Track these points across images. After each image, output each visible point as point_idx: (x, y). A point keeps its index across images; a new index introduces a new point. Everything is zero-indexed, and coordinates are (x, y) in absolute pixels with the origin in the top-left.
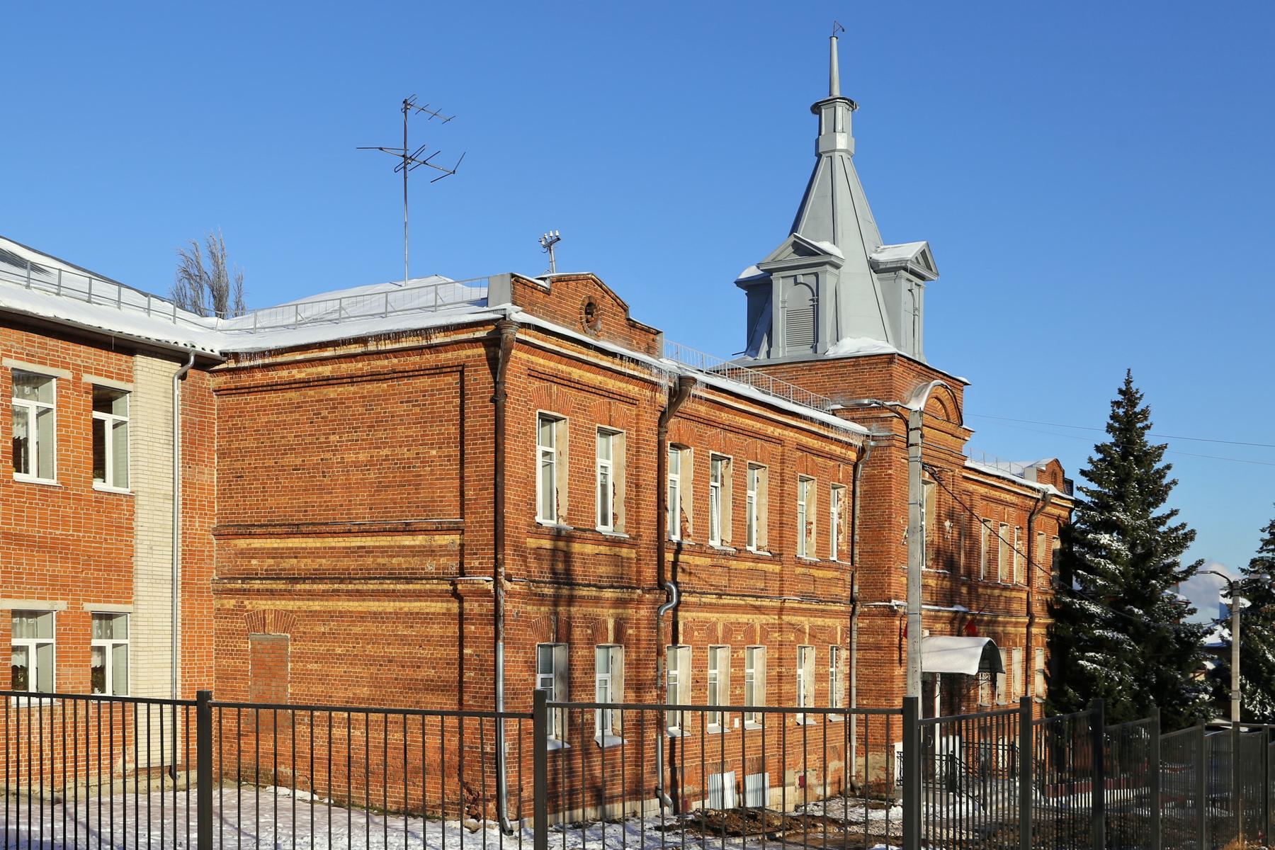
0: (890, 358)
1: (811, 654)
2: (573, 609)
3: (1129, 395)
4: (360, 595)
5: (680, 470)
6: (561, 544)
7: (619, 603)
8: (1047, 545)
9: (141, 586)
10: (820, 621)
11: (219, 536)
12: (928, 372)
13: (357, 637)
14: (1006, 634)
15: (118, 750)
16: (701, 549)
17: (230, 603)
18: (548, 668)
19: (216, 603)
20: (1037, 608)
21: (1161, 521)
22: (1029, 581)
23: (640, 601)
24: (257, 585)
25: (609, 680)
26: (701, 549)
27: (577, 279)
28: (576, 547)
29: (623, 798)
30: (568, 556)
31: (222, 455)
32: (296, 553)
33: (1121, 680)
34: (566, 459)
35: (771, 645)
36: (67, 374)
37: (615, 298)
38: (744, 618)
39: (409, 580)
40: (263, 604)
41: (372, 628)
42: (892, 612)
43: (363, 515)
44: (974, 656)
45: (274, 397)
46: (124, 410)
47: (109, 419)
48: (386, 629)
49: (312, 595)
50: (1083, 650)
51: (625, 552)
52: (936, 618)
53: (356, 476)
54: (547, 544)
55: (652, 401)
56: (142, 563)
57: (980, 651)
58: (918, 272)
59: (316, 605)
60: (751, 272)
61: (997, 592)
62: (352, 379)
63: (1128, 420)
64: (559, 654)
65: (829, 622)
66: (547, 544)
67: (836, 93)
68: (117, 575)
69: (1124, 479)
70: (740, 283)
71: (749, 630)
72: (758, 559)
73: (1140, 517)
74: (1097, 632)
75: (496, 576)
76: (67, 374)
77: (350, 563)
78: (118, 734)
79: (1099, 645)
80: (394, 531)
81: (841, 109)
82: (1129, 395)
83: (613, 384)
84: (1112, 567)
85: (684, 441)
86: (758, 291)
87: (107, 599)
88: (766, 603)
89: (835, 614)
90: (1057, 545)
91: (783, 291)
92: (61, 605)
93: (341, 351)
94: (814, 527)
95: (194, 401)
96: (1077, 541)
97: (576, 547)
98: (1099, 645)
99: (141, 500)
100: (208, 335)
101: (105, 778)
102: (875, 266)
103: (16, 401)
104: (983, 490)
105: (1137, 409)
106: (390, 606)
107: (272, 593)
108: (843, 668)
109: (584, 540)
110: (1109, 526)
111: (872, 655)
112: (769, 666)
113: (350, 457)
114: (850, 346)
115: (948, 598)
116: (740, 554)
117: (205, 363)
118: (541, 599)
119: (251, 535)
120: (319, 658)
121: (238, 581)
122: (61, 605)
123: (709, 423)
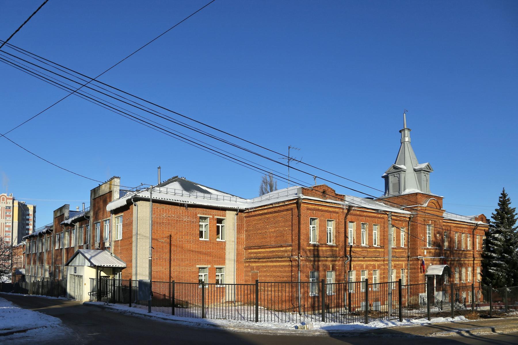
0: (417, 194)
1: (395, 271)
2: (320, 263)
3: (504, 195)
4: (272, 262)
5: (352, 228)
6: (316, 248)
7: (332, 261)
8: (479, 240)
9: (227, 261)
10: (397, 263)
11: (245, 249)
12: (429, 196)
13: (272, 271)
14: (465, 264)
15: (221, 297)
16: (358, 247)
17: (247, 264)
18: (313, 277)
19: (245, 265)
20: (477, 255)
21: (515, 229)
22: (473, 248)
23: (339, 260)
24: (252, 260)
25: (331, 278)
26: (358, 247)
27: (320, 186)
28: (320, 248)
29: (334, 308)
30: (318, 251)
31: (246, 231)
32: (260, 253)
33: (502, 275)
34: (318, 228)
35: (381, 269)
36: (211, 217)
37: (331, 189)
38: (372, 263)
39: (282, 258)
40: (254, 264)
41: (274, 269)
42: (418, 259)
43: (273, 244)
44: (441, 270)
45: (256, 218)
46: (225, 223)
47: (220, 225)
48: (277, 269)
49: (263, 262)
50: (490, 267)
51: (335, 249)
52: (434, 260)
53: (272, 235)
54: (312, 248)
55: (343, 212)
56: (227, 257)
57: (443, 268)
58: (428, 170)
59: (264, 264)
60: (385, 174)
61: (461, 252)
62: (271, 213)
63: (504, 201)
64: (316, 274)
65: (400, 263)
66: (312, 248)
67: (405, 127)
68: (222, 259)
69: (503, 218)
70: (383, 177)
71: (374, 266)
72: (376, 248)
73: (508, 229)
74: (494, 262)
75: (298, 256)
76: (211, 217)
77: (270, 254)
78: (221, 294)
79: (495, 265)
80: (279, 247)
81: (406, 131)
82: (504, 195)
83: (330, 209)
84: (499, 243)
85: (353, 221)
86: (386, 178)
87: (219, 264)
88: (379, 259)
89: (403, 261)
90: (484, 238)
91: (391, 178)
92: (209, 266)
93: (268, 207)
94: (395, 239)
95: (239, 220)
96: (491, 237)
97: (320, 248)
98: (495, 265)
99: (227, 242)
100: (242, 204)
101: (219, 303)
102: (415, 170)
103: (200, 223)
104: (454, 225)
105: (506, 199)
106: (278, 264)
107: (255, 262)
108: (406, 274)
109: (322, 246)
110: (499, 232)
111: (413, 271)
112: (381, 274)
113: (271, 230)
114: (408, 191)
115: (436, 255)
116: (371, 247)
117: (242, 211)
118: (311, 261)
119: (251, 249)
120: (264, 276)
121: (249, 260)
122: (209, 266)
123: (360, 216)
